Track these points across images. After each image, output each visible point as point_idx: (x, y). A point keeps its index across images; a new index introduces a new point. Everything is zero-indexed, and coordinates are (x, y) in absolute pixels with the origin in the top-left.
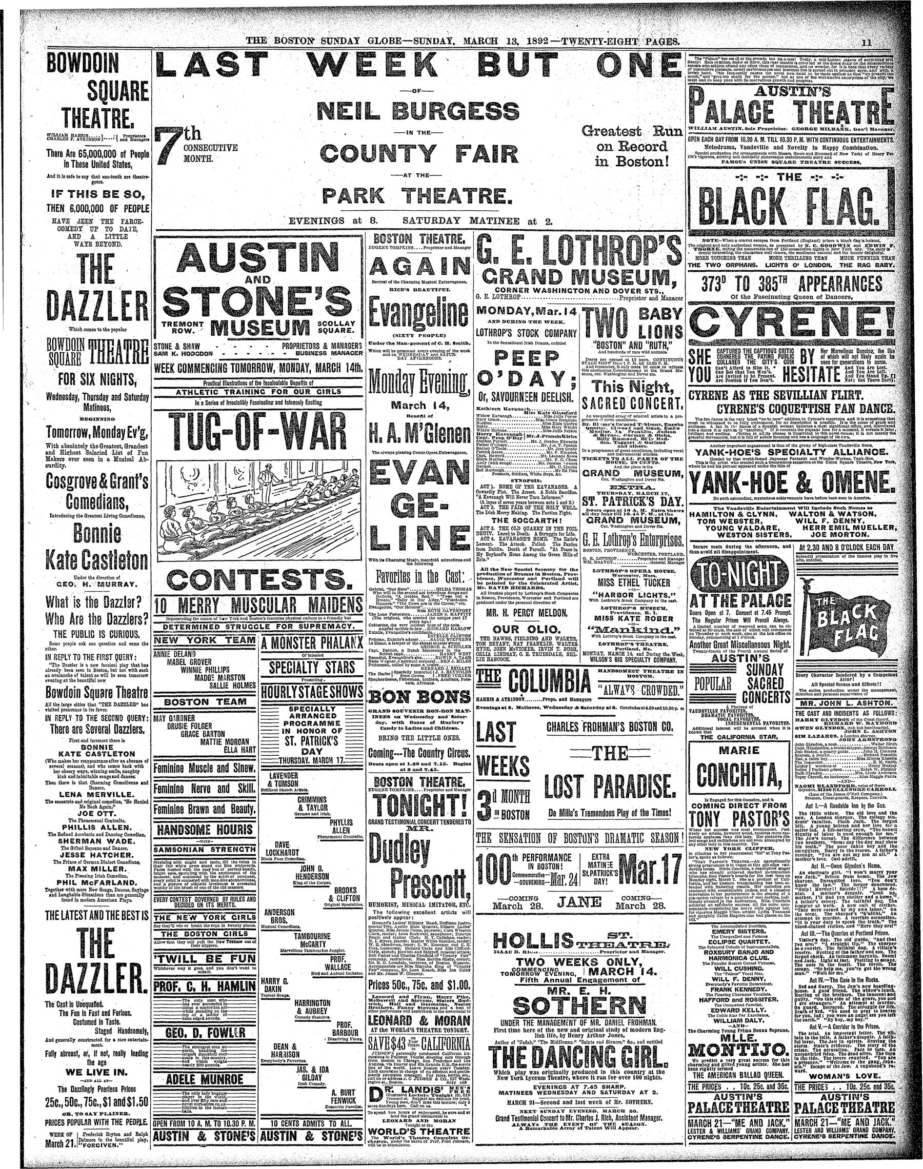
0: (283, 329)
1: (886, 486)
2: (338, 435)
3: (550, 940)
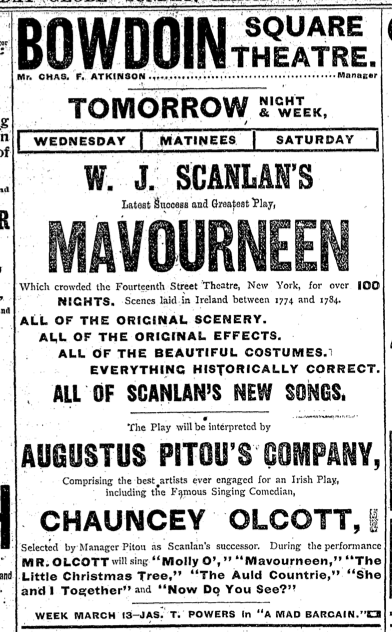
2: (220, 254)
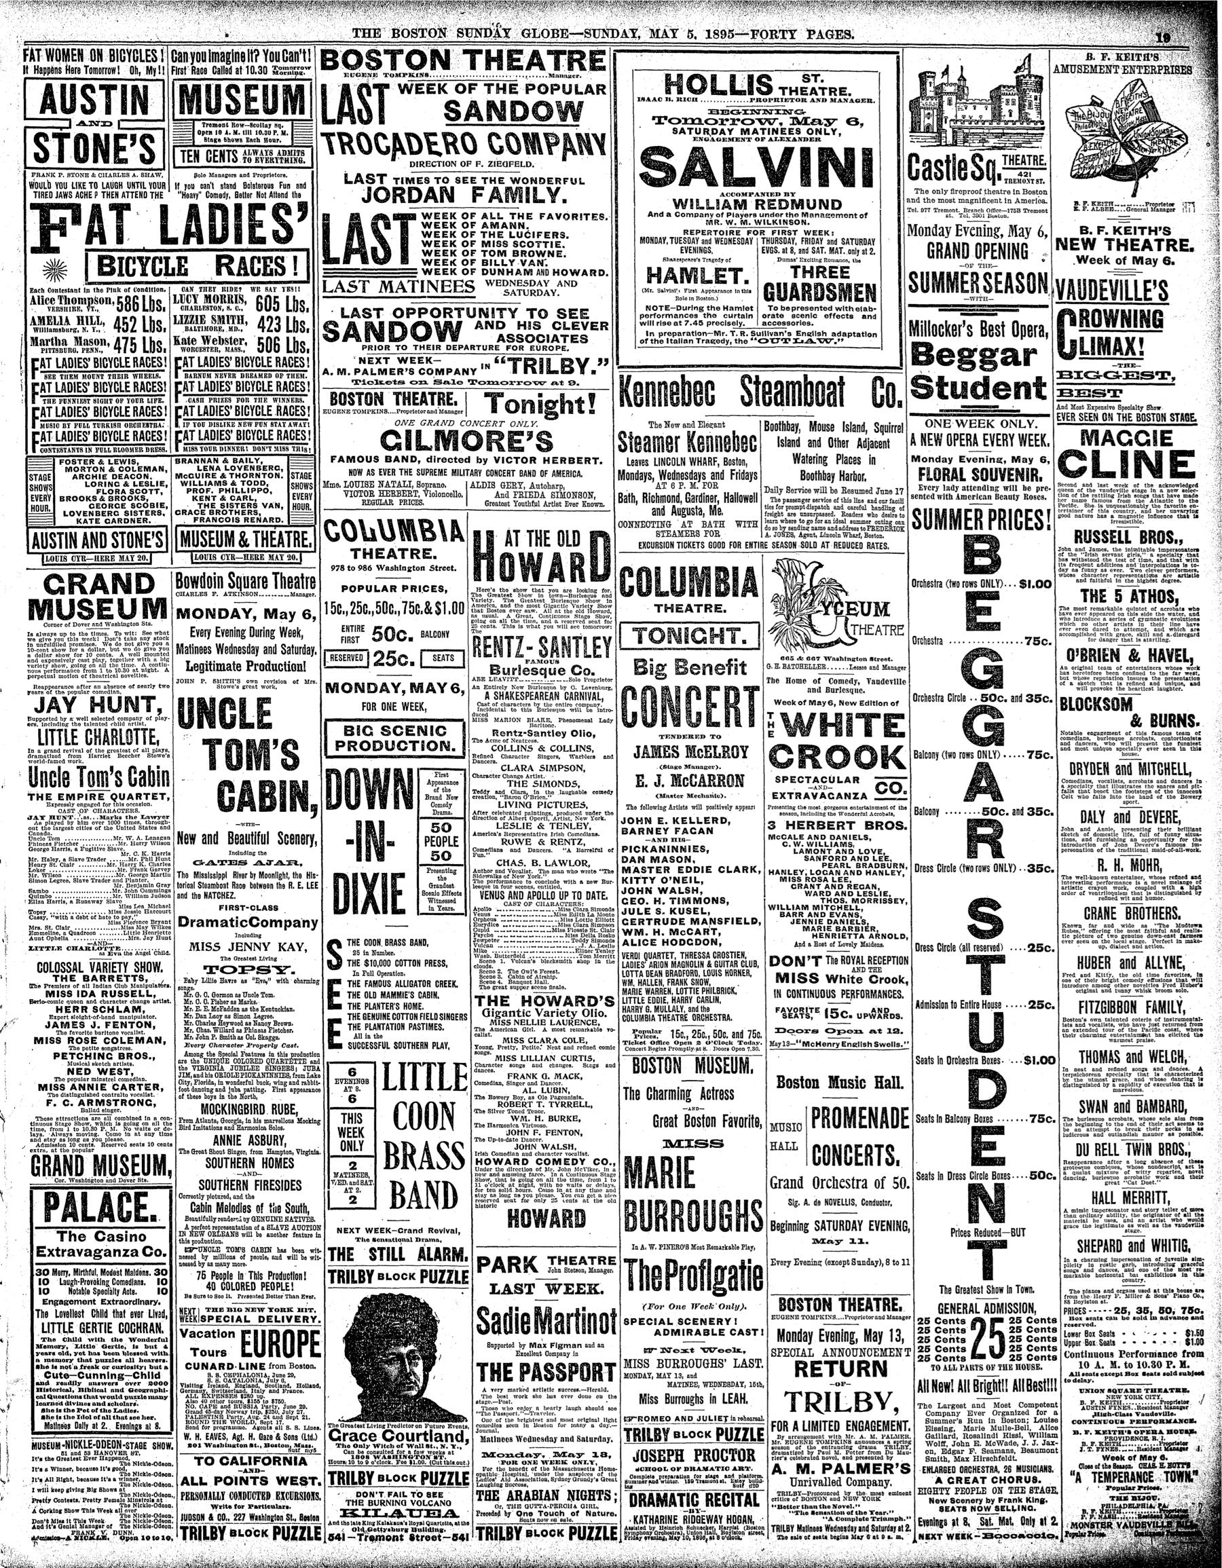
0: (128, 611)
1: (143, 1213)
3: (741, 84)
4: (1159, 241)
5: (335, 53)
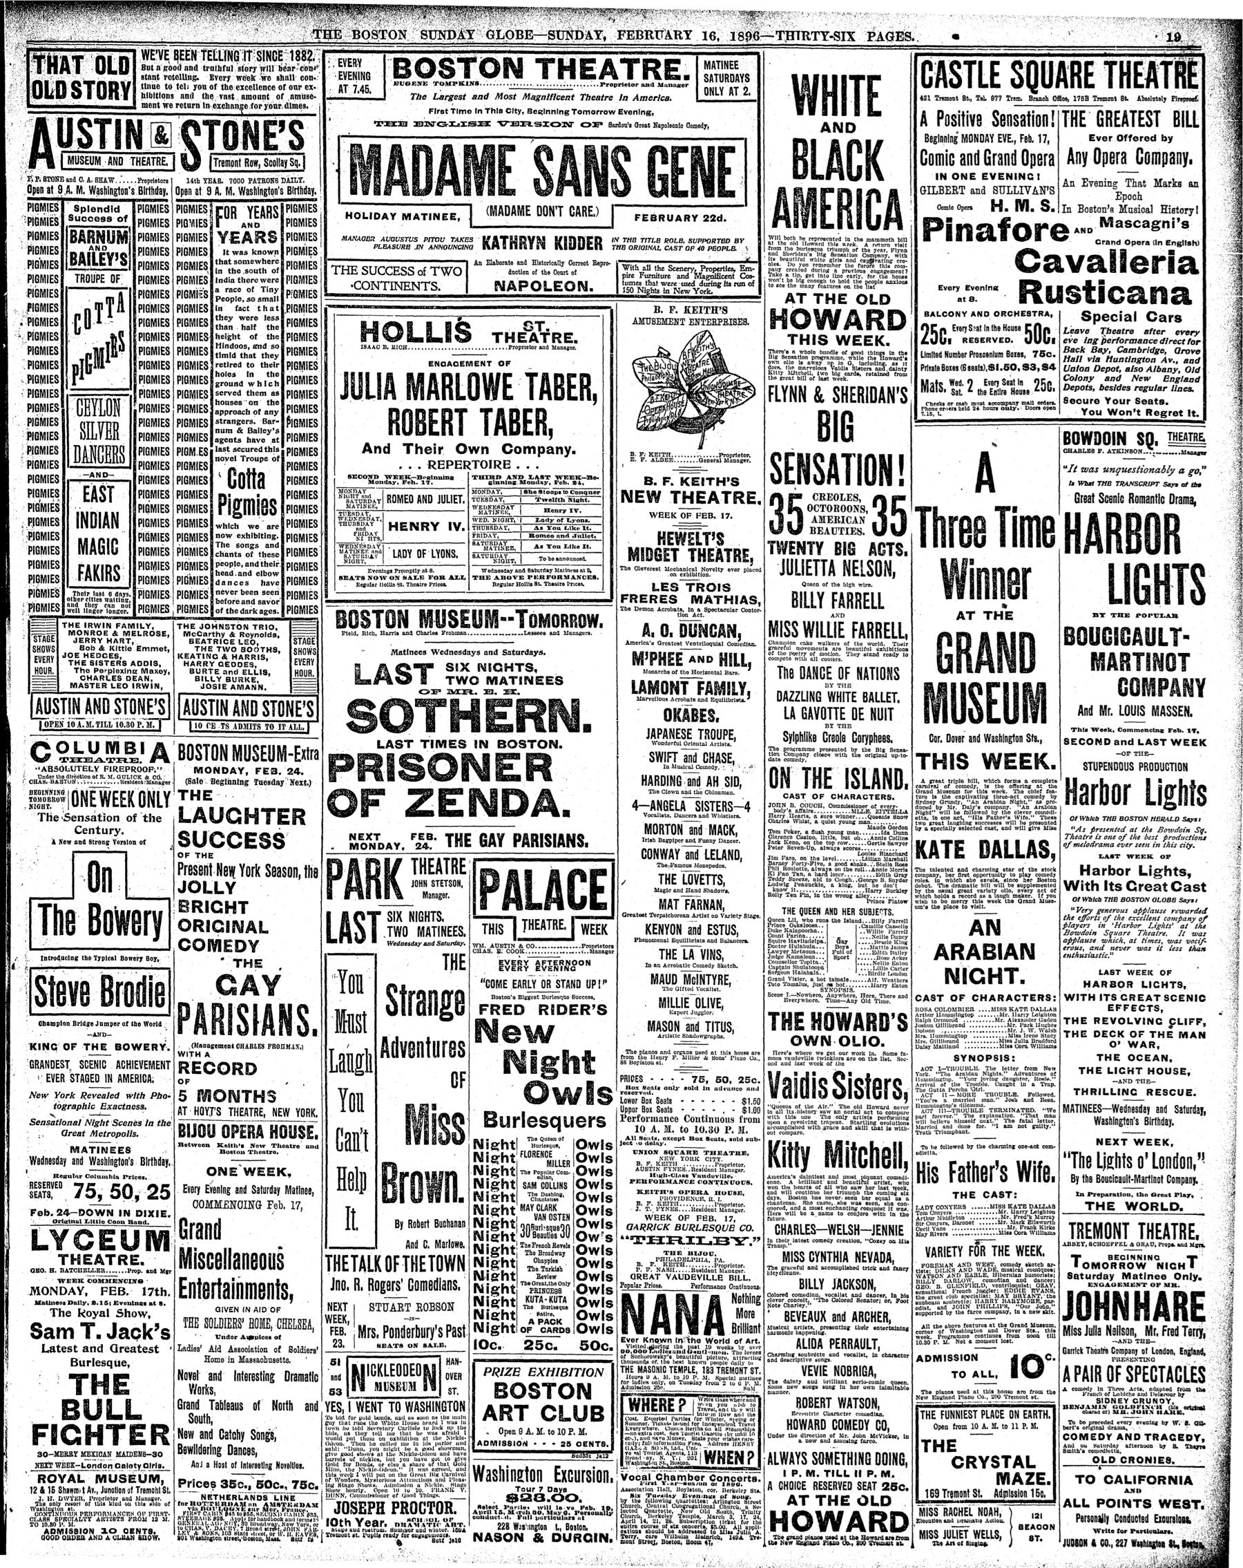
4: (726, 493)
5: (408, 62)
